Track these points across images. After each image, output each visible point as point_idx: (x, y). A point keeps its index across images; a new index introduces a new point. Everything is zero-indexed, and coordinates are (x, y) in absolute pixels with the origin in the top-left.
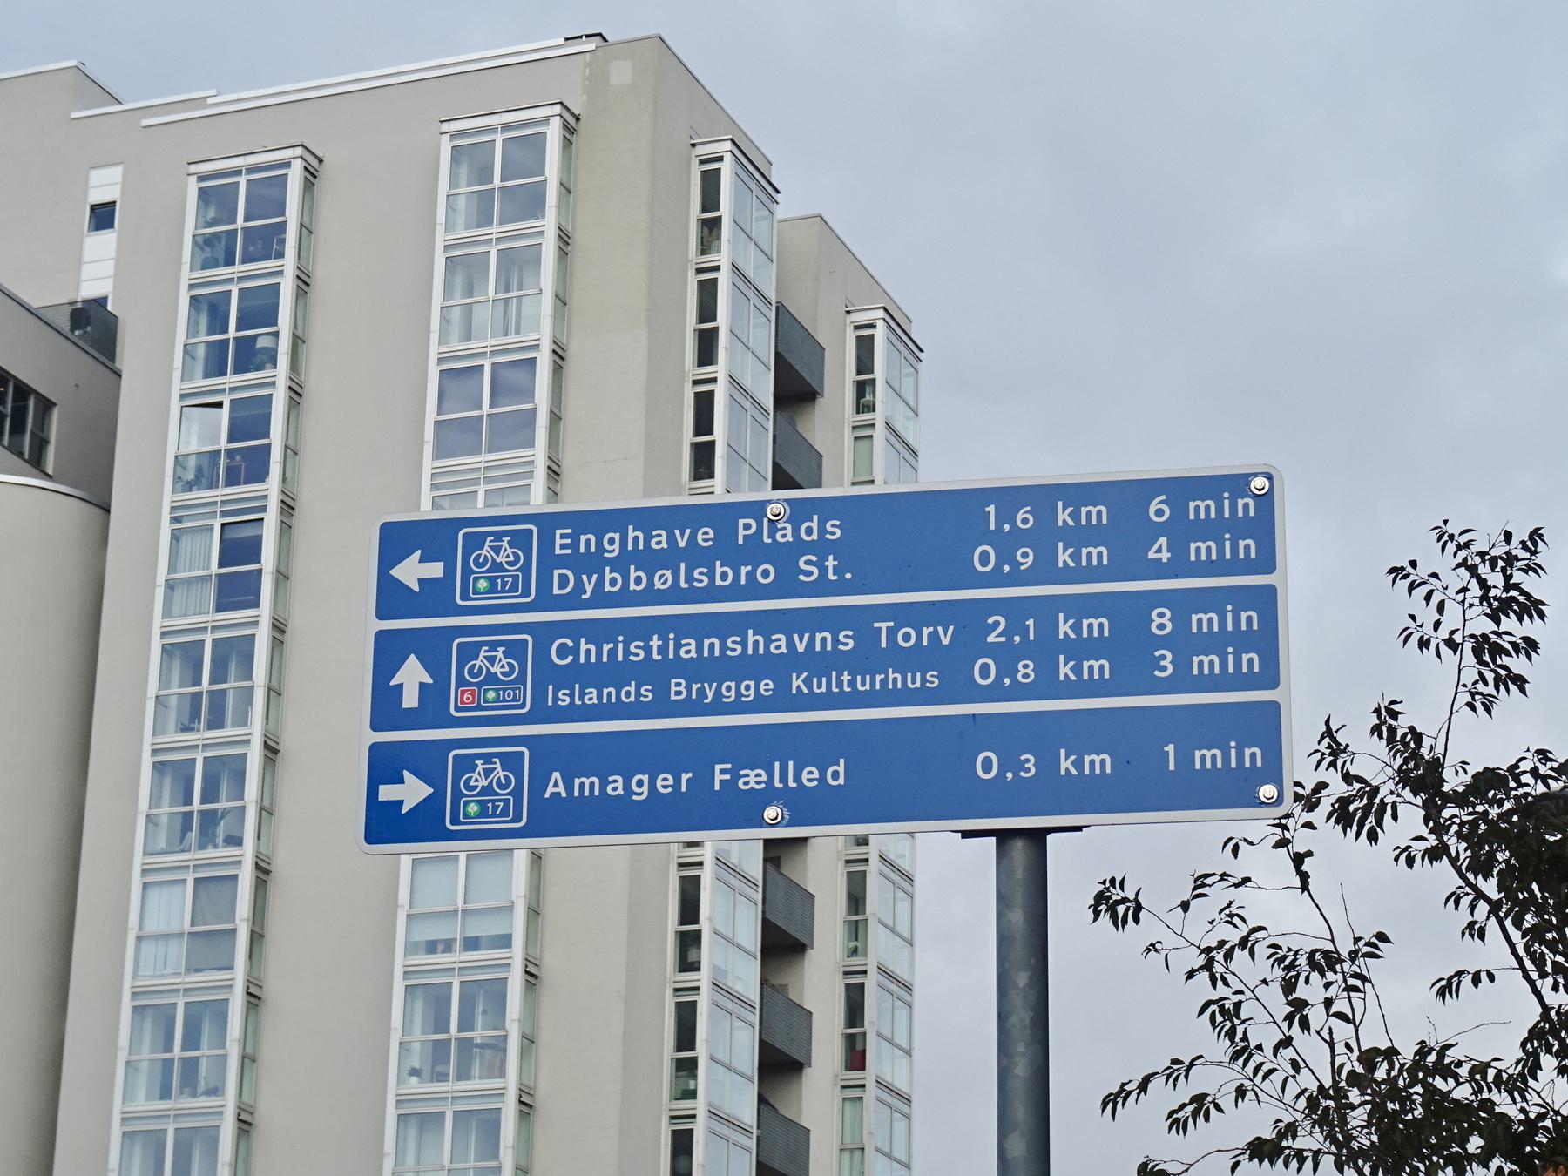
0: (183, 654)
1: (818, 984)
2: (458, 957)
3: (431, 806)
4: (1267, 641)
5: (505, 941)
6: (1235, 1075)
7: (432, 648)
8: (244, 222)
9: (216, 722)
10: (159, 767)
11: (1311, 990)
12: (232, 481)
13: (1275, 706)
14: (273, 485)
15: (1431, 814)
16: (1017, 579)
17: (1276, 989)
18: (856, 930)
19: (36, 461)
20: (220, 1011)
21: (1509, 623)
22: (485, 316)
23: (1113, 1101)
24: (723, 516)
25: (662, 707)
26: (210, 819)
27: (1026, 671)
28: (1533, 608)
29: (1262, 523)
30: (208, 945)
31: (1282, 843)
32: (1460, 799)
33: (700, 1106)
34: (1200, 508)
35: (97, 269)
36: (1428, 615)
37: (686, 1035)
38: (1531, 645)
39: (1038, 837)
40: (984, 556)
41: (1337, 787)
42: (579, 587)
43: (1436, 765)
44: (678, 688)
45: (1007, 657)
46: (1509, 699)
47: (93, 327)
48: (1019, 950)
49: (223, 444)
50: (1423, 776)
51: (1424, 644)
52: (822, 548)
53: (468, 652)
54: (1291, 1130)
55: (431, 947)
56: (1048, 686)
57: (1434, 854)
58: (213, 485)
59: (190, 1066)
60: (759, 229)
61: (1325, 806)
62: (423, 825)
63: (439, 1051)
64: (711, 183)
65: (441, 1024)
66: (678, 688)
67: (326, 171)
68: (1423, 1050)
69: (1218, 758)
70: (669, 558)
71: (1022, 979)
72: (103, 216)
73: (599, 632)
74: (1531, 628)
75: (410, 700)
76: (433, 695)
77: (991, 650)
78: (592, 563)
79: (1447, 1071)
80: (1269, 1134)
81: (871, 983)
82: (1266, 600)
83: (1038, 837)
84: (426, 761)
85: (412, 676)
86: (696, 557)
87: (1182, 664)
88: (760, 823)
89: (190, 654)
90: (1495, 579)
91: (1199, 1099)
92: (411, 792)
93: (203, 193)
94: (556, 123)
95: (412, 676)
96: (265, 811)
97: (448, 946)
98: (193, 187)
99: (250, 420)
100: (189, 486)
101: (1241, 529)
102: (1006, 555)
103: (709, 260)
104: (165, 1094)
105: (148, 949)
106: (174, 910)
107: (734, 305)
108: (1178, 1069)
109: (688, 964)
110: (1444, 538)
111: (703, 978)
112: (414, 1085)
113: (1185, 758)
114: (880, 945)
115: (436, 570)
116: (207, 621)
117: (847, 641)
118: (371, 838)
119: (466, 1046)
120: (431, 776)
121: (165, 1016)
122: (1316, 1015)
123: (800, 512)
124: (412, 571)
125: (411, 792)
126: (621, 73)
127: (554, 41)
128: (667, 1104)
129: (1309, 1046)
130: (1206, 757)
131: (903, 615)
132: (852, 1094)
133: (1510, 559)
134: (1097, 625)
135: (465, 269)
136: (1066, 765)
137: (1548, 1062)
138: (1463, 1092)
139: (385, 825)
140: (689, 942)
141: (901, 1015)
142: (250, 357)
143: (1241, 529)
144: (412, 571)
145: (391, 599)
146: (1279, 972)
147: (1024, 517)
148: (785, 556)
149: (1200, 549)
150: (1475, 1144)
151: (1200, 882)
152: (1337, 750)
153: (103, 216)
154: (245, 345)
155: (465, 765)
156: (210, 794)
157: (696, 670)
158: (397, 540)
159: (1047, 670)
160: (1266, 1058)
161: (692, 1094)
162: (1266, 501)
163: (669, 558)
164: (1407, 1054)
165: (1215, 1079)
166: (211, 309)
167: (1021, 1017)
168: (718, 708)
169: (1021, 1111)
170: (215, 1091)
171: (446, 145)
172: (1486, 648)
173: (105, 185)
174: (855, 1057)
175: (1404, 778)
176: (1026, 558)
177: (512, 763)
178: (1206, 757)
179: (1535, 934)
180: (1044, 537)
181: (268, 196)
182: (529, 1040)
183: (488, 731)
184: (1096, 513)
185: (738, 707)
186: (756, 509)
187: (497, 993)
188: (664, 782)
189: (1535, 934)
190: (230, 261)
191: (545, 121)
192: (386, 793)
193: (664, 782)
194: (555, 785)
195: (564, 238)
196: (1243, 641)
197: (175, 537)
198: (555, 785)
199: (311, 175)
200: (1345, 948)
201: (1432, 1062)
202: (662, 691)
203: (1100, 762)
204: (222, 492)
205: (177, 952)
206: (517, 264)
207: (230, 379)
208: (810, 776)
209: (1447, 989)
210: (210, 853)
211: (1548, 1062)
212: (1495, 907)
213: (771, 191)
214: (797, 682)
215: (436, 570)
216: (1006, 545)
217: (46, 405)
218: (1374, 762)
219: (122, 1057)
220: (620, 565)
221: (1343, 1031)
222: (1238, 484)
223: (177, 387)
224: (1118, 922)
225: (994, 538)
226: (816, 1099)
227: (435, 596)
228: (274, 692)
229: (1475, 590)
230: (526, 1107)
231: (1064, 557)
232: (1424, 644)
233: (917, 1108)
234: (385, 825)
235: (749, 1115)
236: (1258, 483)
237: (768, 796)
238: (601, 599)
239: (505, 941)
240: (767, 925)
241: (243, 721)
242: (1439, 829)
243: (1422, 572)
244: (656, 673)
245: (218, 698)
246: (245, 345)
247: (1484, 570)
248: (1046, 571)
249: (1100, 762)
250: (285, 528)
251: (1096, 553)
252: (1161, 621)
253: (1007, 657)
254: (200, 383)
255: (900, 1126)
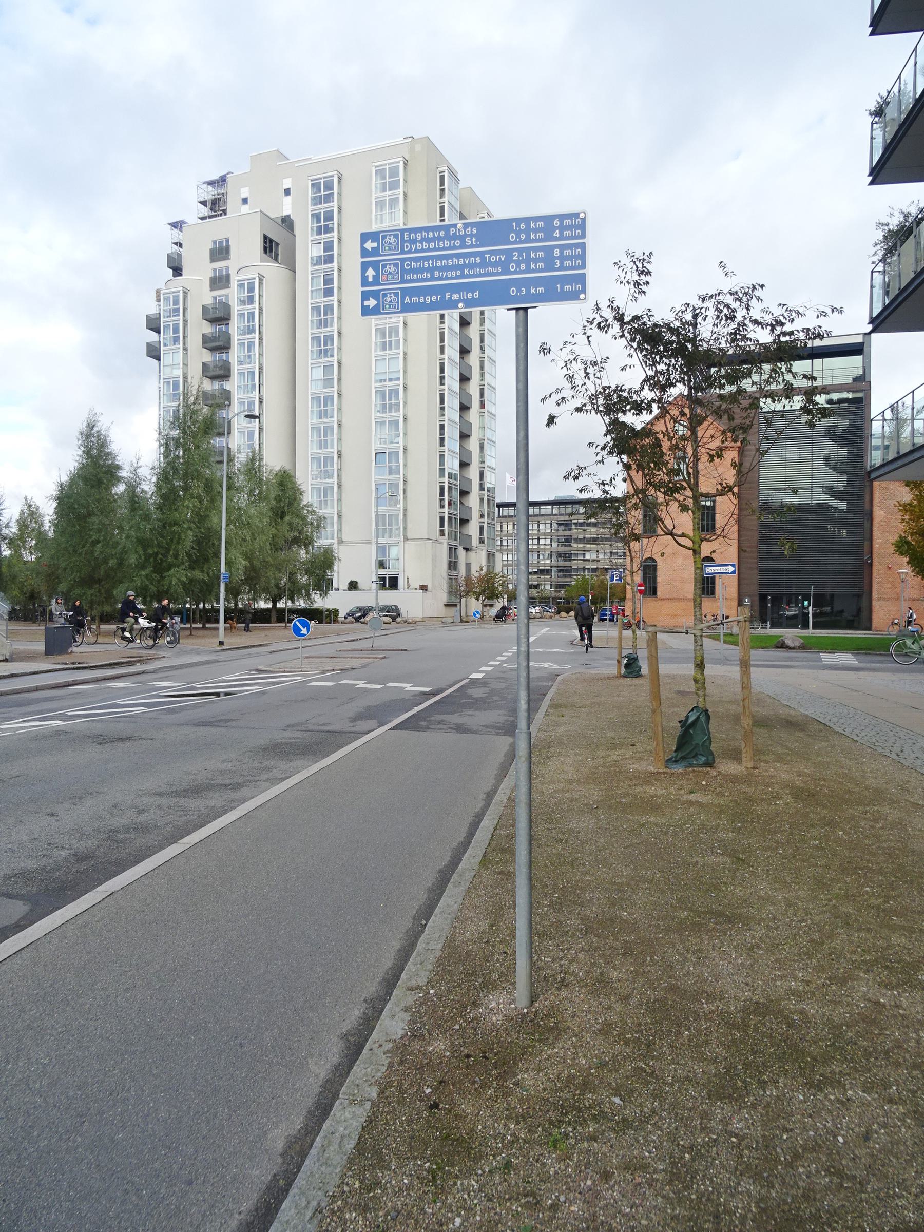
0: (316, 309)
1: (473, 388)
2: (387, 383)
3: (377, 306)
4: (583, 257)
5: (398, 379)
6: (572, 392)
7: (375, 265)
8: (324, 191)
9: (326, 326)
10: (312, 338)
11: (590, 370)
12: (325, 263)
13: (584, 274)
14: (335, 297)
15: (621, 327)
16: (521, 242)
17: (582, 371)
18: (482, 375)
19: (276, 259)
20: (332, 398)
21: (642, 277)
22: (386, 217)
23: (543, 400)
24: (447, 228)
25: (433, 278)
26: (326, 351)
27: (523, 267)
28: (648, 273)
29: (582, 226)
30: (328, 382)
31: (585, 333)
32: (628, 323)
33: (446, 418)
34: (567, 222)
35: (287, 207)
36: (623, 275)
37: (442, 401)
38: (648, 283)
39: (526, 309)
40: (512, 237)
41: (599, 320)
42: (411, 248)
43: (623, 315)
44: (436, 274)
45: (518, 263)
46: (641, 297)
47: (287, 222)
48: (521, 338)
49: (322, 253)
50: (620, 318)
51: (621, 282)
52: (472, 236)
53: (384, 266)
54: (585, 405)
55: (381, 381)
56: (528, 270)
57: (622, 336)
58: (320, 264)
59: (326, 411)
60: (455, 191)
61: (596, 323)
62: (375, 311)
63: (384, 406)
64: (442, 178)
65: (384, 399)
66: (436, 274)
67: (344, 178)
68: (617, 387)
69: (570, 287)
70: (433, 240)
71: (522, 345)
72: (287, 192)
73: (416, 260)
74: (648, 278)
75: (370, 279)
76: (376, 278)
77: (514, 261)
78: (414, 242)
79: (621, 390)
80: (580, 406)
81: (486, 388)
82: (584, 276)
83: (526, 309)
84: (375, 295)
85: (370, 273)
86: (440, 239)
87: (562, 263)
88: (457, 308)
89: (319, 339)
90: (640, 265)
91: (563, 398)
92: (372, 303)
93: (313, 185)
94: (402, 163)
95: (370, 273)
96: (339, 349)
97: (385, 380)
98: (310, 183)
99: (328, 247)
100: (315, 265)
101: (577, 227)
102: (518, 236)
103: (442, 200)
104: (320, 418)
105: (313, 383)
106: (319, 373)
107: (449, 338)
108: (558, 391)
109: (442, 384)
110: (628, 254)
111: (446, 387)
112: (379, 415)
113: (562, 288)
114: (488, 379)
115: (375, 245)
116: (322, 301)
117: (478, 260)
118: (363, 314)
119: (390, 405)
120: (377, 299)
121: (319, 399)
122: (591, 376)
123: (466, 226)
124: (369, 245)
125: (372, 303)
126: (418, 148)
127: (400, 140)
128: (438, 418)
129: (590, 385)
130: (567, 288)
131: (492, 253)
132: (482, 414)
133: (644, 260)
134: (541, 254)
135: (380, 204)
136: (533, 291)
137: (646, 388)
138: (625, 394)
139: (366, 311)
140: (442, 378)
141: (493, 395)
142: (328, 230)
143: (577, 227)
144: (369, 245)
145: (364, 253)
146: (583, 366)
147: (523, 226)
148: (462, 238)
149: (567, 233)
150: (628, 407)
151: (565, 343)
152: (598, 309)
153: (287, 192)
154: (326, 227)
155: (385, 295)
156: (325, 344)
157: (441, 269)
158: (365, 237)
159: (528, 266)
160: (579, 388)
161: (444, 415)
162: (584, 220)
163: (433, 240)
164: (613, 387)
165: (568, 393)
166: (316, 217)
167: (522, 354)
168: (447, 278)
169: (522, 378)
170: (332, 417)
171: (374, 170)
172: (637, 284)
173: (287, 183)
174: (482, 406)
175: (615, 318)
176: (523, 237)
177: (396, 294)
178: (567, 288)
179: (645, 356)
180: (528, 231)
181: (329, 186)
182: (405, 403)
183: (391, 286)
184: (540, 224)
185: (452, 278)
186: (455, 226)
187: (397, 391)
188: (434, 298)
189: (645, 356)
190: (320, 204)
191: (399, 162)
192: (366, 303)
193: (434, 298)
194: (407, 300)
195: (405, 195)
196: (577, 257)
197: (312, 278)
198: (407, 300)
199: (339, 178)
200: (599, 360)
201: (619, 389)
202: (432, 275)
203: (541, 290)
204: (323, 266)
205: (321, 384)
206: (394, 202)
207: (323, 236)
208: (470, 295)
209: (623, 369)
210: (326, 359)
211: (646, 388)
212: (636, 349)
213: (457, 180)
214: (466, 271)
215: (375, 245)
216: (518, 234)
217: (277, 244)
218: (609, 315)
219: (310, 439)
220: (421, 242)
221: (598, 381)
222: (577, 215)
223: (310, 238)
224: (545, 354)
225: (515, 232)
226: (473, 415)
227: (375, 252)
228: (339, 318)
229: (635, 268)
230: (405, 419)
231: (532, 236)
232: (621, 282)
233: (497, 471)
234: (366, 311)
235: (458, 420)
236: (582, 215)
237: (460, 301)
238: (416, 251)
239: (398, 379)
240: (461, 374)
241: (332, 326)
242: (623, 331)
243: (622, 264)
244: (431, 270)
245: (326, 320)
246: (326, 227)
247: (637, 263)
248: (528, 240)
249: (541, 290)
250: (339, 276)
251: (541, 235)
252: (557, 252)
253: (518, 263)
254: (316, 237)
255: (493, 422)
